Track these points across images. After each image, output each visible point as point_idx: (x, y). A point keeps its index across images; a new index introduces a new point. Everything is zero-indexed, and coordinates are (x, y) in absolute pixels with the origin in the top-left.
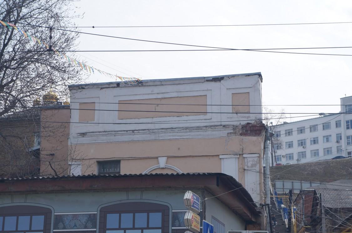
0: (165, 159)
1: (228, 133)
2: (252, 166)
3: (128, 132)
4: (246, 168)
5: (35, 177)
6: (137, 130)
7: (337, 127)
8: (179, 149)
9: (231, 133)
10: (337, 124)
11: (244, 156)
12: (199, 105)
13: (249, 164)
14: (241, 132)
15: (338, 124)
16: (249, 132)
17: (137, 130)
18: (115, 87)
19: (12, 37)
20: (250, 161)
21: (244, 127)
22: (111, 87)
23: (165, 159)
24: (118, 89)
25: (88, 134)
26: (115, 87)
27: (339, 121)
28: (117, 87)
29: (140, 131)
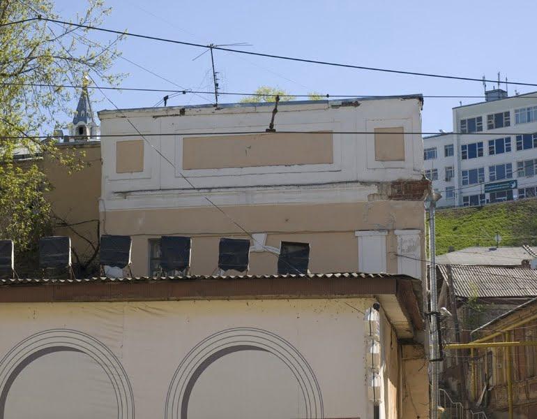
0: (263, 236)
1: (369, 196)
2: (409, 250)
3: (200, 191)
4: (399, 252)
5: (37, 279)
6: (216, 188)
7: (446, 155)
8: (287, 220)
9: (374, 195)
10: (446, 150)
11: (396, 232)
12: (317, 145)
13: (405, 247)
14: (390, 193)
15: (449, 151)
16: (403, 193)
17: (216, 188)
18: (176, 115)
19: (66, 138)
20: (406, 241)
21: (395, 184)
22: (173, 115)
23: (263, 236)
24: (182, 117)
25: (132, 193)
26: (176, 115)
27: (450, 146)
28: (180, 115)
29: (222, 190)
